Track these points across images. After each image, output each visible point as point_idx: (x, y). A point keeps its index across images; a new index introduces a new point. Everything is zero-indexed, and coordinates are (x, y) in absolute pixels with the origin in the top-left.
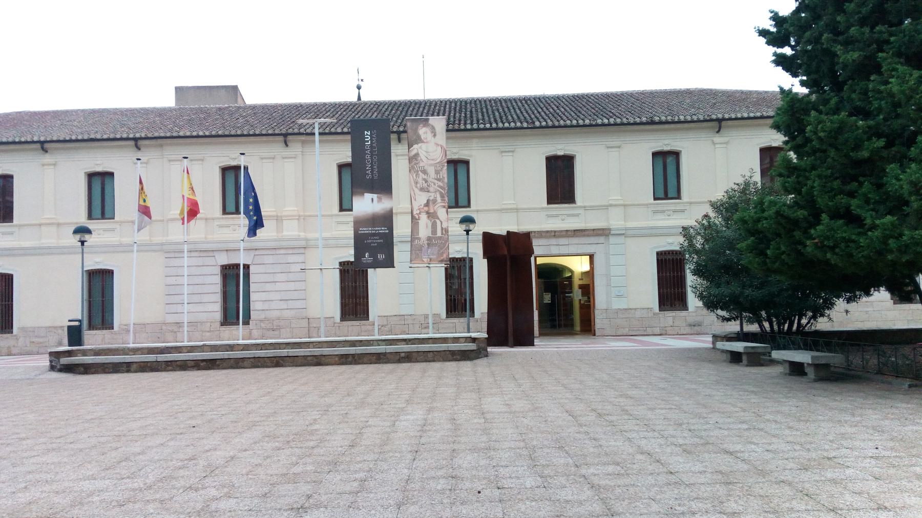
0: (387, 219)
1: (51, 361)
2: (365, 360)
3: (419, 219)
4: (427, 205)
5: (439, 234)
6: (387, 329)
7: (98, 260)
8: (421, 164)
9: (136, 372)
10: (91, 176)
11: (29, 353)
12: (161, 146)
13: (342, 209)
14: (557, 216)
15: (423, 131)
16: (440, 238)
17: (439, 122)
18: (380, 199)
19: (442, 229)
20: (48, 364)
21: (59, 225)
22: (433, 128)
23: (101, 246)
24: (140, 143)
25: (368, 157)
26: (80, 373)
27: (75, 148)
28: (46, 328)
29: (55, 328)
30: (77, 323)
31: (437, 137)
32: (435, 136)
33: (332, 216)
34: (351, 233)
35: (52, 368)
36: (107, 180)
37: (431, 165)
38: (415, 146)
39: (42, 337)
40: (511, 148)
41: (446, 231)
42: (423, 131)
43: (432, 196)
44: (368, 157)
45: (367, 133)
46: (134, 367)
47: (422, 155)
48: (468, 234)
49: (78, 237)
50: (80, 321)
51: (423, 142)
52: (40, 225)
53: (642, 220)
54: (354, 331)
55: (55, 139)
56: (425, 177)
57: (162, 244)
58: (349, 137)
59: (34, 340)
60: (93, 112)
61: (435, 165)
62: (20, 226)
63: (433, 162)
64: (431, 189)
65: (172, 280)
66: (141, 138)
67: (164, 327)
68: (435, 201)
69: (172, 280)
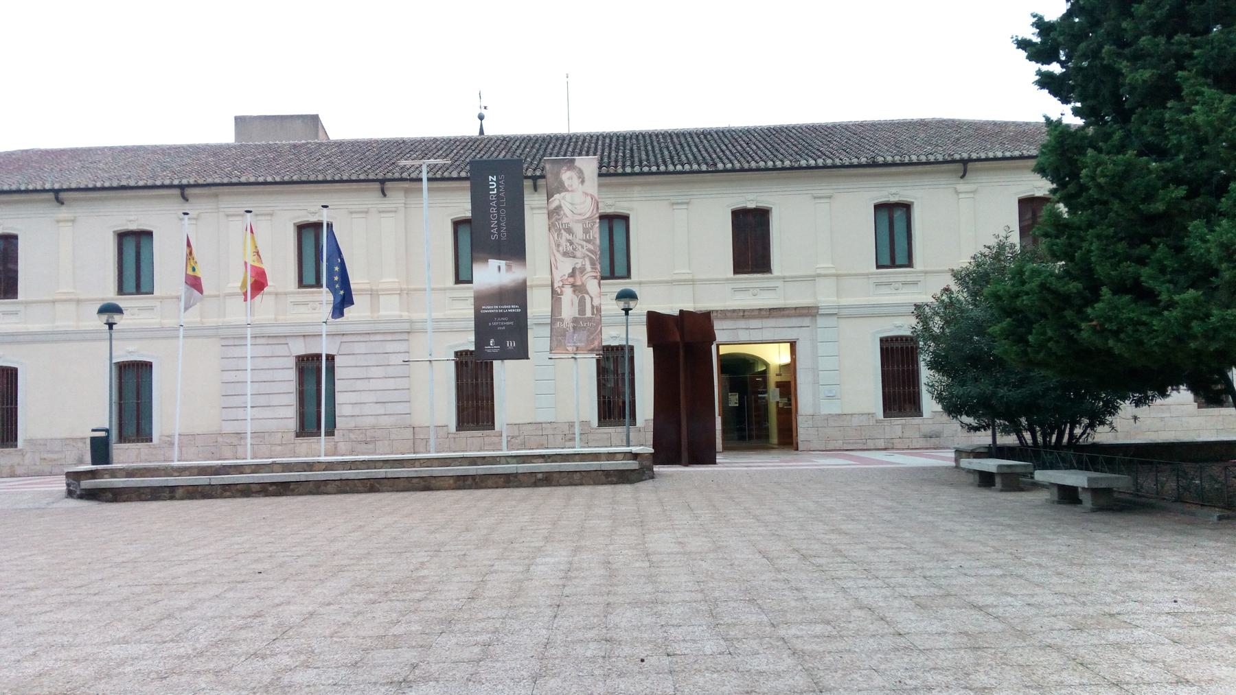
0: (519, 294)
1: (68, 485)
2: (490, 482)
3: (562, 294)
4: (573, 275)
5: (588, 314)
6: (518, 441)
7: (131, 349)
8: (565, 220)
9: (182, 499)
10: (122, 236)
11: (40, 474)
12: (216, 195)
13: (458, 281)
14: (747, 290)
15: (567, 176)
16: (590, 319)
17: (588, 164)
18: (509, 268)
19: (593, 307)
20: (64, 488)
21: (79, 301)
22: (580, 172)
23: (135, 330)
24: (188, 191)
25: (493, 210)
26: (107, 501)
27: (100, 199)
28: (62, 439)
29: (74, 439)
30: (103, 434)
31: (586, 183)
32: (583, 182)
33: (445, 289)
34: (470, 313)
35: (70, 494)
36: (144, 241)
37: (578, 221)
38: (557, 196)
39: (57, 452)
40: (684, 199)
41: (597, 310)
42: (567, 176)
43: (579, 263)
44: (493, 210)
45: (492, 178)
46: (180, 492)
47: (566, 209)
48: (627, 314)
49: (105, 317)
50: (107, 431)
51: (567, 191)
52: (54, 302)
53: (861, 295)
54: (474, 444)
55: (73, 186)
56: (570, 237)
57: (217, 328)
58: (467, 184)
59: (45, 456)
60: (125, 150)
61: (583, 222)
62: (27, 303)
63: (580, 218)
64: (578, 254)
65: (231, 376)
66: (189, 186)
67: (220, 439)
68: (583, 270)
69: (231, 376)
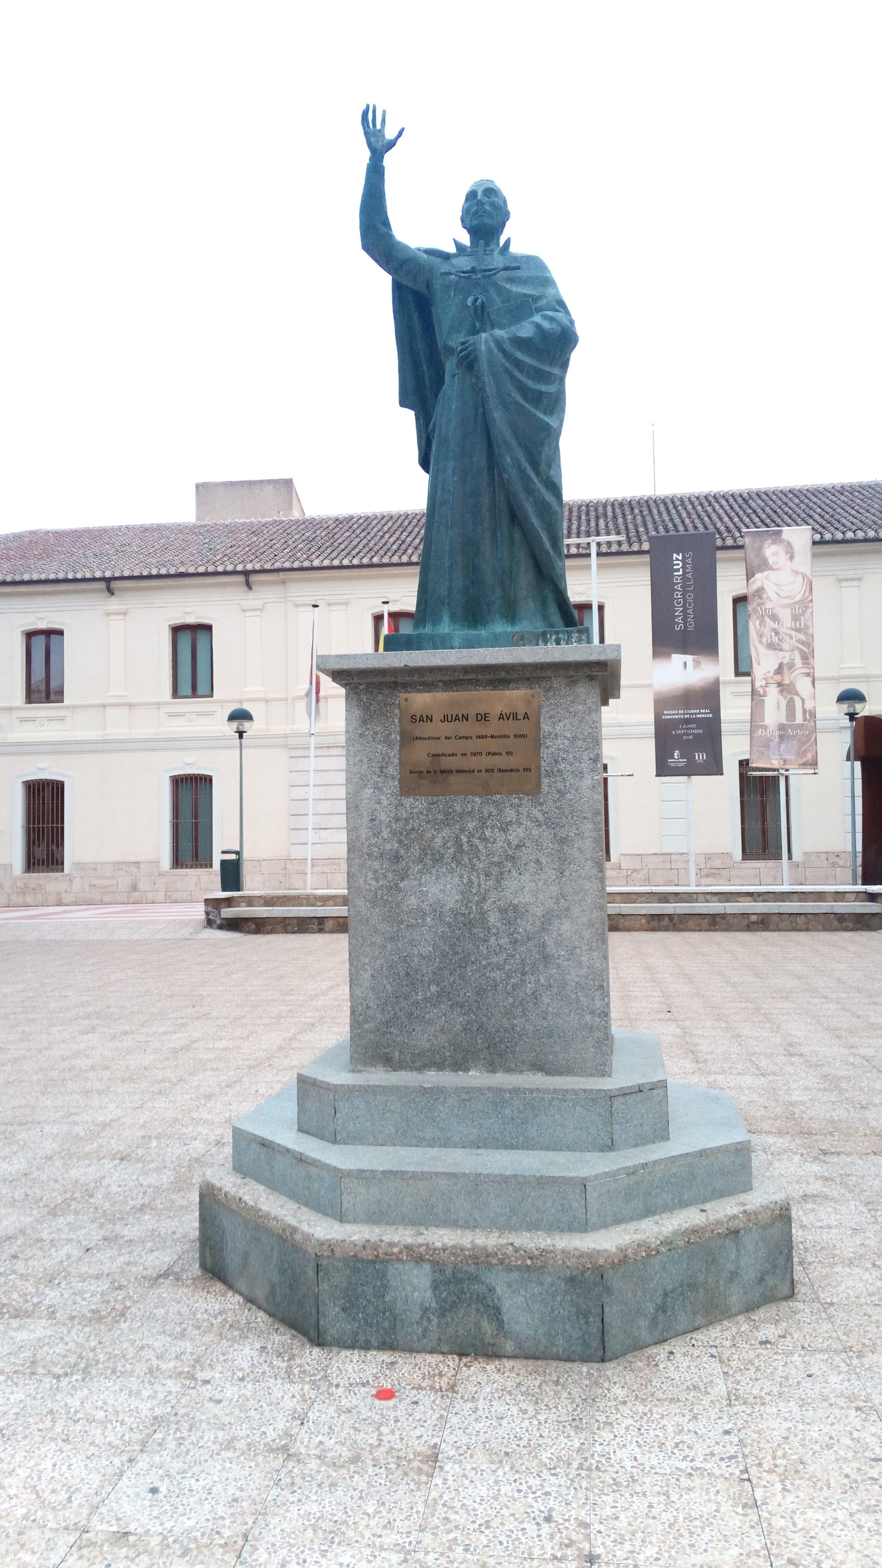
0: (709, 696)
1: (207, 913)
2: (691, 924)
3: (765, 695)
4: (779, 671)
5: (799, 719)
6: (641, 875)
7: (189, 760)
8: (769, 605)
9: (332, 932)
10: (177, 630)
11: (90, 903)
12: (284, 582)
13: (738, 673)
14: (182, 715)
15: (771, 551)
16: (801, 727)
17: (799, 536)
18: (697, 664)
19: (804, 711)
20: (203, 916)
21: (131, 706)
22: (789, 545)
23: (192, 739)
24: (253, 578)
25: (678, 595)
26: (250, 932)
27: (150, 589)
28: (114, 863)
29: (128, 863)
30: (233, 857)
31: (796, 559)
32: (792, 558)
33: (10, 709)
34: (651, 718)
35: (210, 923)
36: (201, 638)
37: (786, 606)
38: (758, 576)
39: (107, 878)
40: (258, 603)
41: (811, 715)
42: (771, 551)
43: (786, 657)
44: (678, 595)
45: (677, 557)
46: (329, 924)
47: (770, 591)
48: (241, 737)
49: (234, 725)
50: (237, 853)
51: (773, 569)
52: (104, 706)
53: (146, 726)
54: (762, 877)
55: (126, 573)
56: (776, 626)
57: (285, 736)
58: (646, 558)
59: (97, 882)
60: (146, 530)
61: (792, 606)
62: (74, 708)
63: (787, 601)
64: (785, 646)
65: (297, 793)
66: (255, 572)
67: (289, 866)
68: (791, 666)
69: (297, 793)
